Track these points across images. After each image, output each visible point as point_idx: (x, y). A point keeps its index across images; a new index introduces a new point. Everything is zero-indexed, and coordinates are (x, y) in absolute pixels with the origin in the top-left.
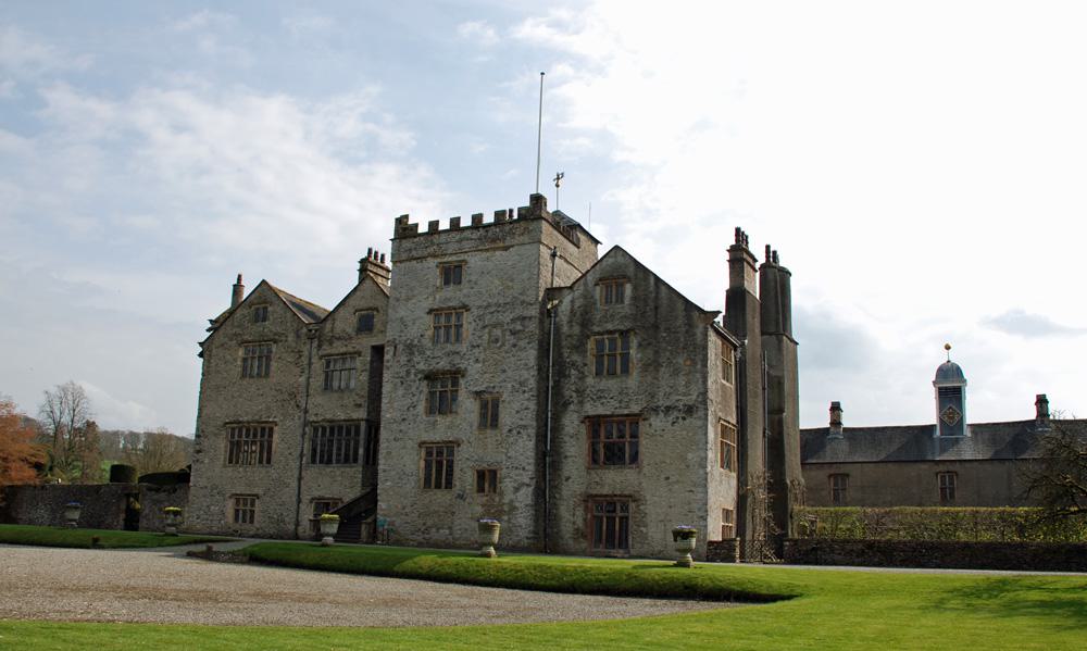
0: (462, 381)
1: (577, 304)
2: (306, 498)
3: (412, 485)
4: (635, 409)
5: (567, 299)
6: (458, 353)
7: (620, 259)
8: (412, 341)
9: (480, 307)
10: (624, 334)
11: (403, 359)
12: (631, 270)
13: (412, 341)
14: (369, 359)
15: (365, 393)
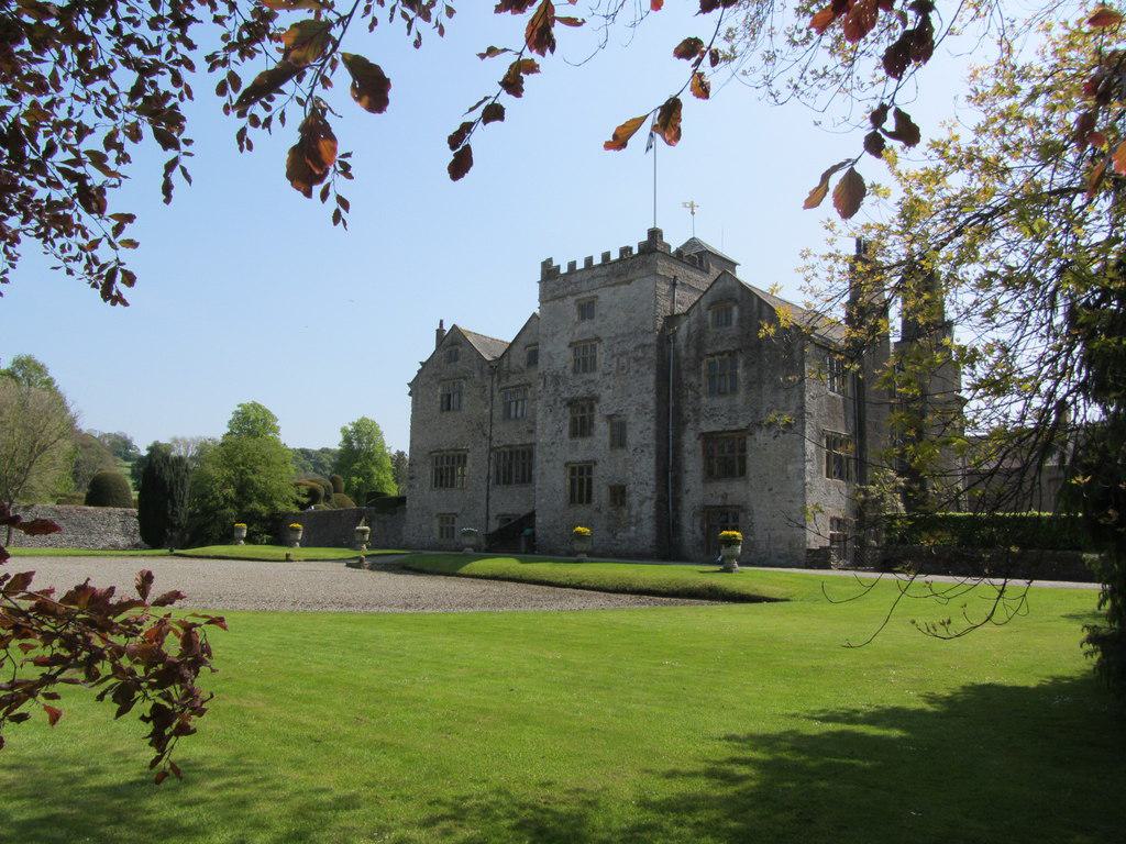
0: (597, 407)
1: (693, 329)
2: (493, 514)
3: (561, 500)
4: (742, 424)
5: (684, 326)
6: (593, 381)
10: (732, 354)
11: (551, 389)
12: (738, 293)
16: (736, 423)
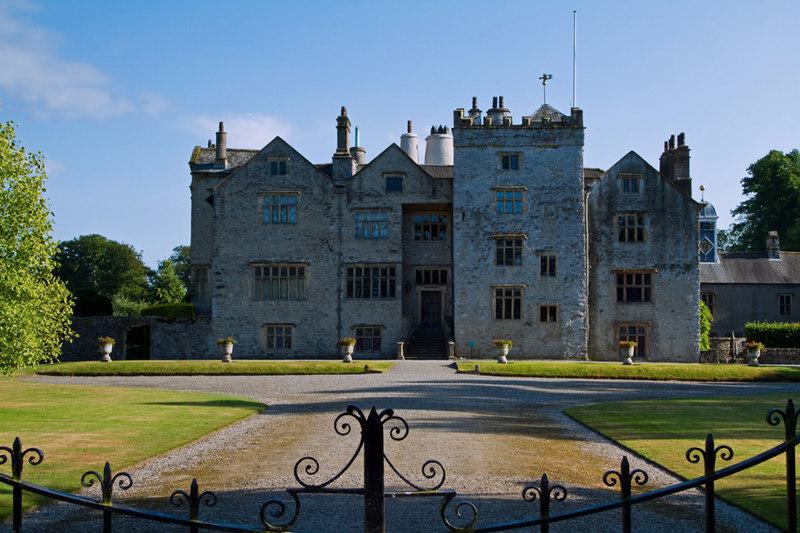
2: (346, 325)
7: (634, 160)
8: (479, 209)
9: (535, 189)
10: (641, 215)
11: (472, 223)
13: (479, 209)
14: (400, 214)
15: (399, 241)
16: (644, 264)
